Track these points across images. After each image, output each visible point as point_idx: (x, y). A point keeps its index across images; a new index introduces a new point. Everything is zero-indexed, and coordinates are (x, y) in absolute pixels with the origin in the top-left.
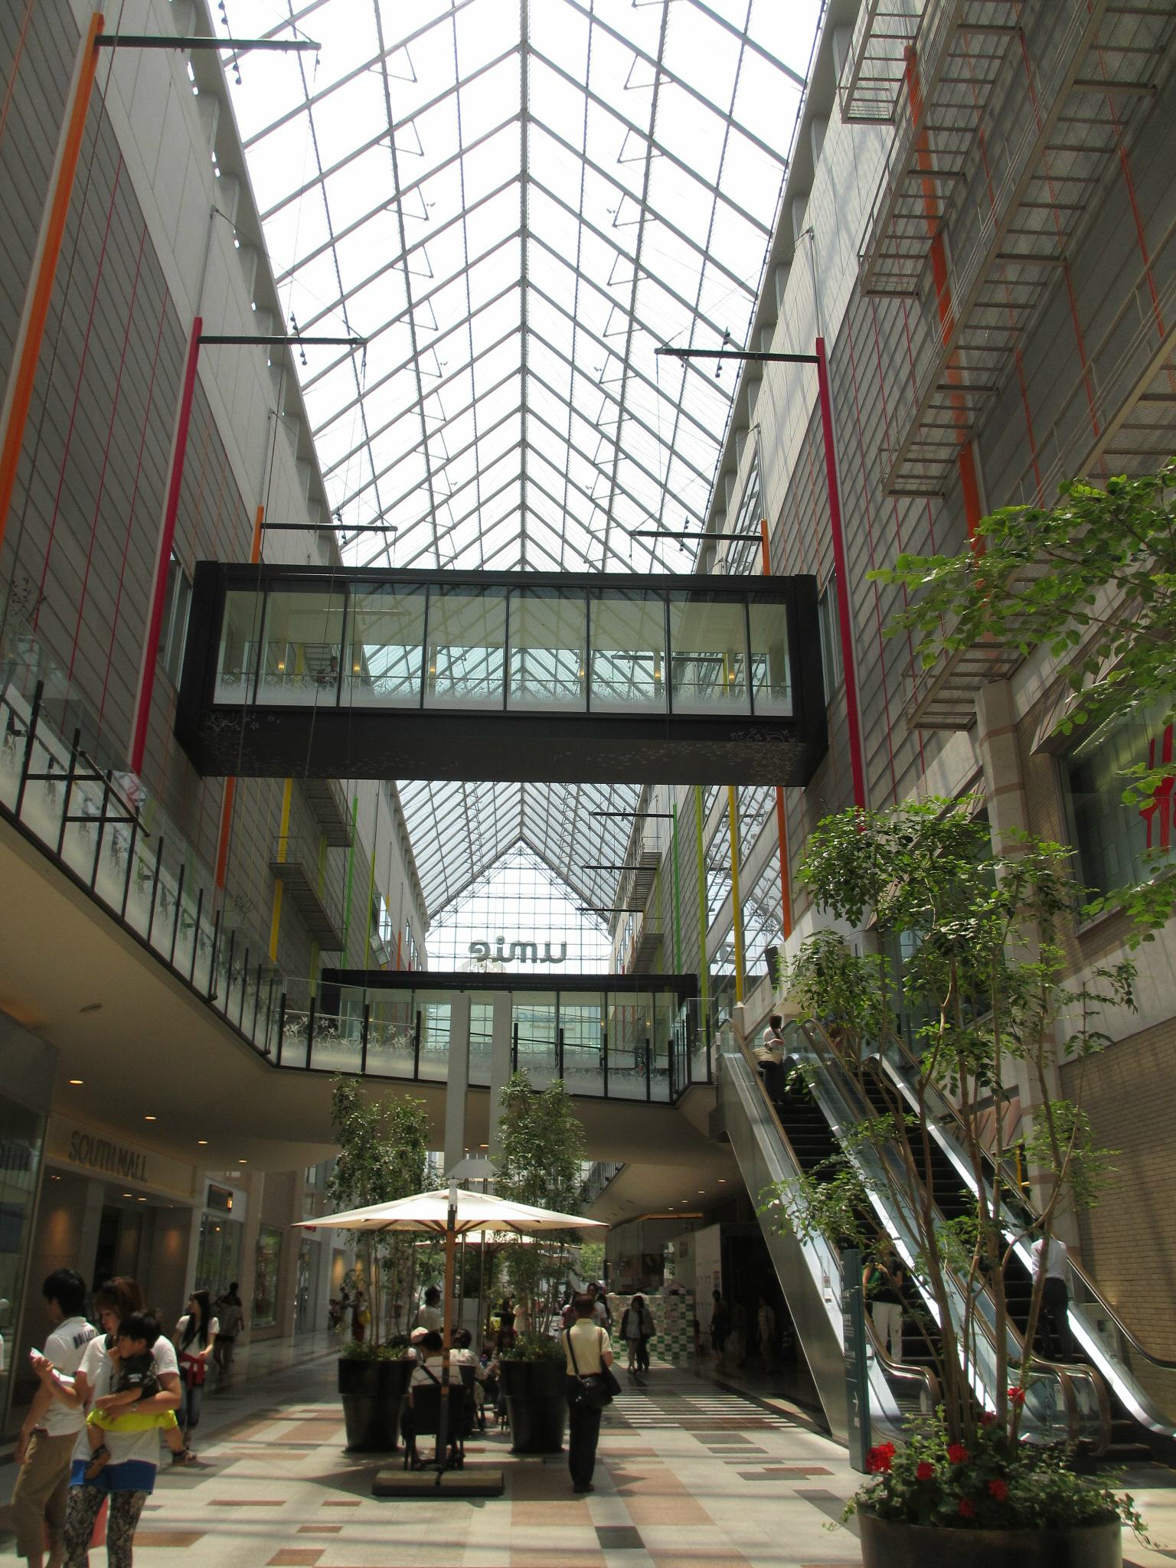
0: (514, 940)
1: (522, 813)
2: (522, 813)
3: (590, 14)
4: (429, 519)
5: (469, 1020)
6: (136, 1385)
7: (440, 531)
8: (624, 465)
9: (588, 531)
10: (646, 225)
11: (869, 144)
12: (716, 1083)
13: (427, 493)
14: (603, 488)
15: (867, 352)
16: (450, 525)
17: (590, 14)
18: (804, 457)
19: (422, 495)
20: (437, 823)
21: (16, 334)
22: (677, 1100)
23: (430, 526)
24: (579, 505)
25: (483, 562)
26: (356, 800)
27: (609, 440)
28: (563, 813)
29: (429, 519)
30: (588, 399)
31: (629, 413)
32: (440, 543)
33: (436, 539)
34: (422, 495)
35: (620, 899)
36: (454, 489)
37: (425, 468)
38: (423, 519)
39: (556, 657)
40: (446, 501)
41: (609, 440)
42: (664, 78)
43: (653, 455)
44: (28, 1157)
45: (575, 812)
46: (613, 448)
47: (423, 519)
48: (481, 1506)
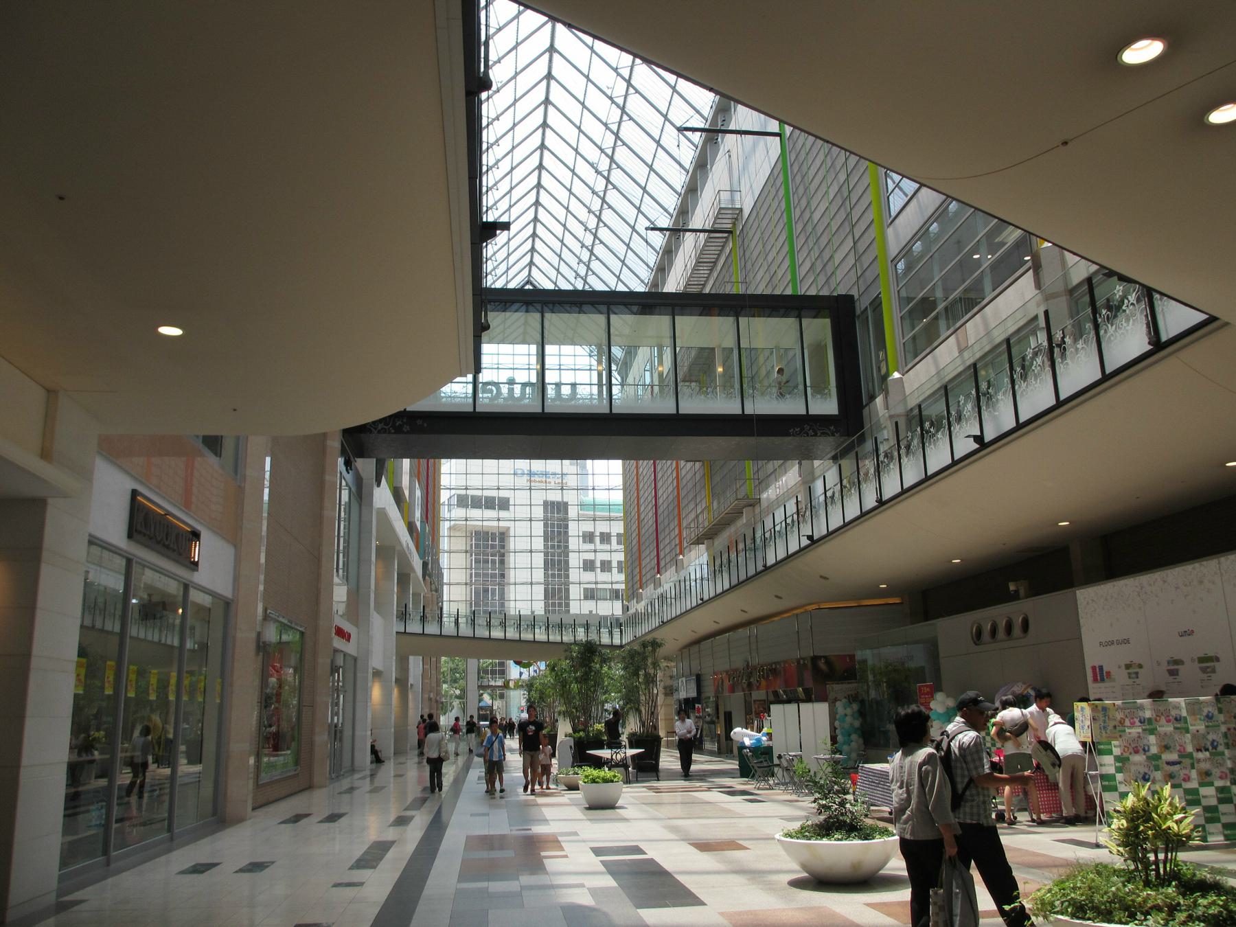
0: (525, 380)
10: (636, 68)
25: (517, 17)
30: (598, 102)
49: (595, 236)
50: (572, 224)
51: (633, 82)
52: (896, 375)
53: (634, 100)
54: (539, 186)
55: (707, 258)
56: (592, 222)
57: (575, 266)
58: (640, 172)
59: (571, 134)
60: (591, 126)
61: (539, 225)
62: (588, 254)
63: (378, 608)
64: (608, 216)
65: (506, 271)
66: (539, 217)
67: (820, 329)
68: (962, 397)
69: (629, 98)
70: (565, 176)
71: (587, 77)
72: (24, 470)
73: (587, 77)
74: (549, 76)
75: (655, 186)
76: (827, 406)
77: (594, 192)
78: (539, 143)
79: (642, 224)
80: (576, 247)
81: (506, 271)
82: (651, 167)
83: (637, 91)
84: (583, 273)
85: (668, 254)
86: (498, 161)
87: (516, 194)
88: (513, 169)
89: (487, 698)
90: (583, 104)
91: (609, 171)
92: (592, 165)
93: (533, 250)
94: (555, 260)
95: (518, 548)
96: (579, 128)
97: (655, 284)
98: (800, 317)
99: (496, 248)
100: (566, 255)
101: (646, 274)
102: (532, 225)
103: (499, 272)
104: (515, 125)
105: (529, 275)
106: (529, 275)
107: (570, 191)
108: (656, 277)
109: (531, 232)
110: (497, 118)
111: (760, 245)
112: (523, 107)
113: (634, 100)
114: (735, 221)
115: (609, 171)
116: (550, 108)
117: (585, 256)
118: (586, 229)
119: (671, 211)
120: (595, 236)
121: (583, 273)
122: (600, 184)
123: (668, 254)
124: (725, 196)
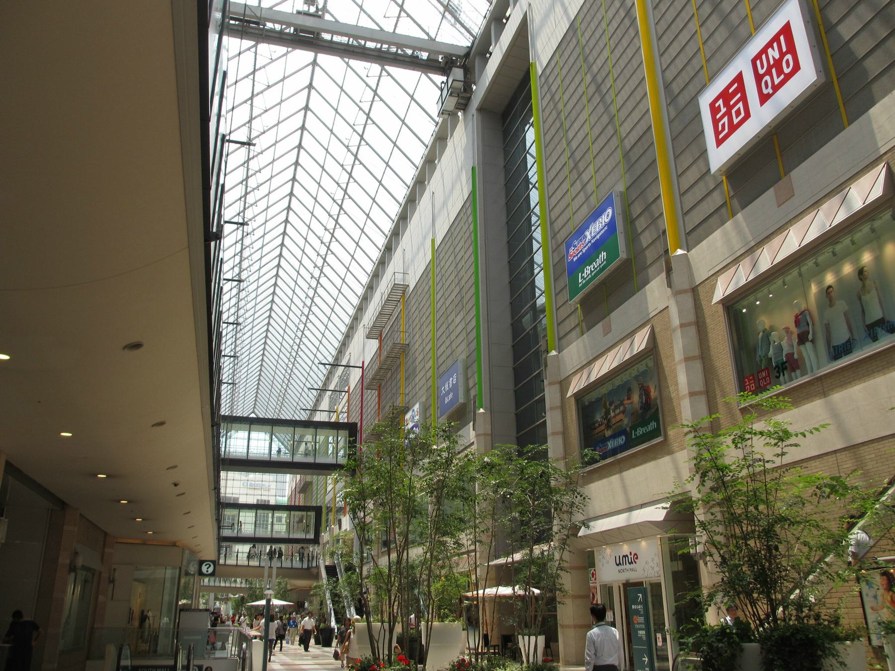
3: (361, 7)
4: (249, 102)
7: (250, 173)
10: (382, 78)
11: (556, 9)
12: (318, 567)
15: (449, 253)
16: (257, 169)
17: (361, 7)
18: (456, 223)
22: (308, 568)
23: (244, 187)
25: (285, 55)
27: (364, 112)
30: (348, 110)
32: (253, 122)
36: (266, 129)
38: (244, 125)
39: (347, 63)
41: (364, 112)
42: (403, 14)
43: (392, 125)
47: (244, 125)
49: (325, 260)
50: (312, 238)
51: (378, 92)
52: (680, 252)
54: (287, 221)
55: (387, 312)
56: (323, 250)
57: (309, 280)
58: (366, 203)
59: (313, 187)
60: (331, 166)
65: (257, 289)
66: (287, 231)
67: (312, 514)
70: (310, 202)
71: (323, 167)
73: (327, 150)
74: (303, 128)
75: (376, 214)
76: (311, 536)
77: (330, 216)
78: (286, 205)
79: (316, 362)
80: (320, 231)
81: (257, 289)
82: (380, 182)
83: (345, 213)
84: (314, 285)
85: (330, 374)
86: (254, 230)
87: (269, 226)
88: (268, 207)
89: (218, 603)
90: (341, 88)
92: (319, 238)
94: (292, 284)
96: (319, 184)
99: (252, 251)
100: (303, 271)
102: (279, 248)
103: (252, 279)
104: (266, 221)
105: (287, 217)
106: (287, 217)
107: (312, 213)
108: (361, 303)
109: (278, 253)
110: (260, 171)
111: (453, 256)
112: (281, 148)
113: (358, 168)
114: (404, 292)
116: (313, 91)
117: (320, 262)
118: (318, 255)
119: (380, 247)
120: (325, 260)
121: (314, 285)
122: (335, 210)
123: (330, 374)
124: (399, 277)
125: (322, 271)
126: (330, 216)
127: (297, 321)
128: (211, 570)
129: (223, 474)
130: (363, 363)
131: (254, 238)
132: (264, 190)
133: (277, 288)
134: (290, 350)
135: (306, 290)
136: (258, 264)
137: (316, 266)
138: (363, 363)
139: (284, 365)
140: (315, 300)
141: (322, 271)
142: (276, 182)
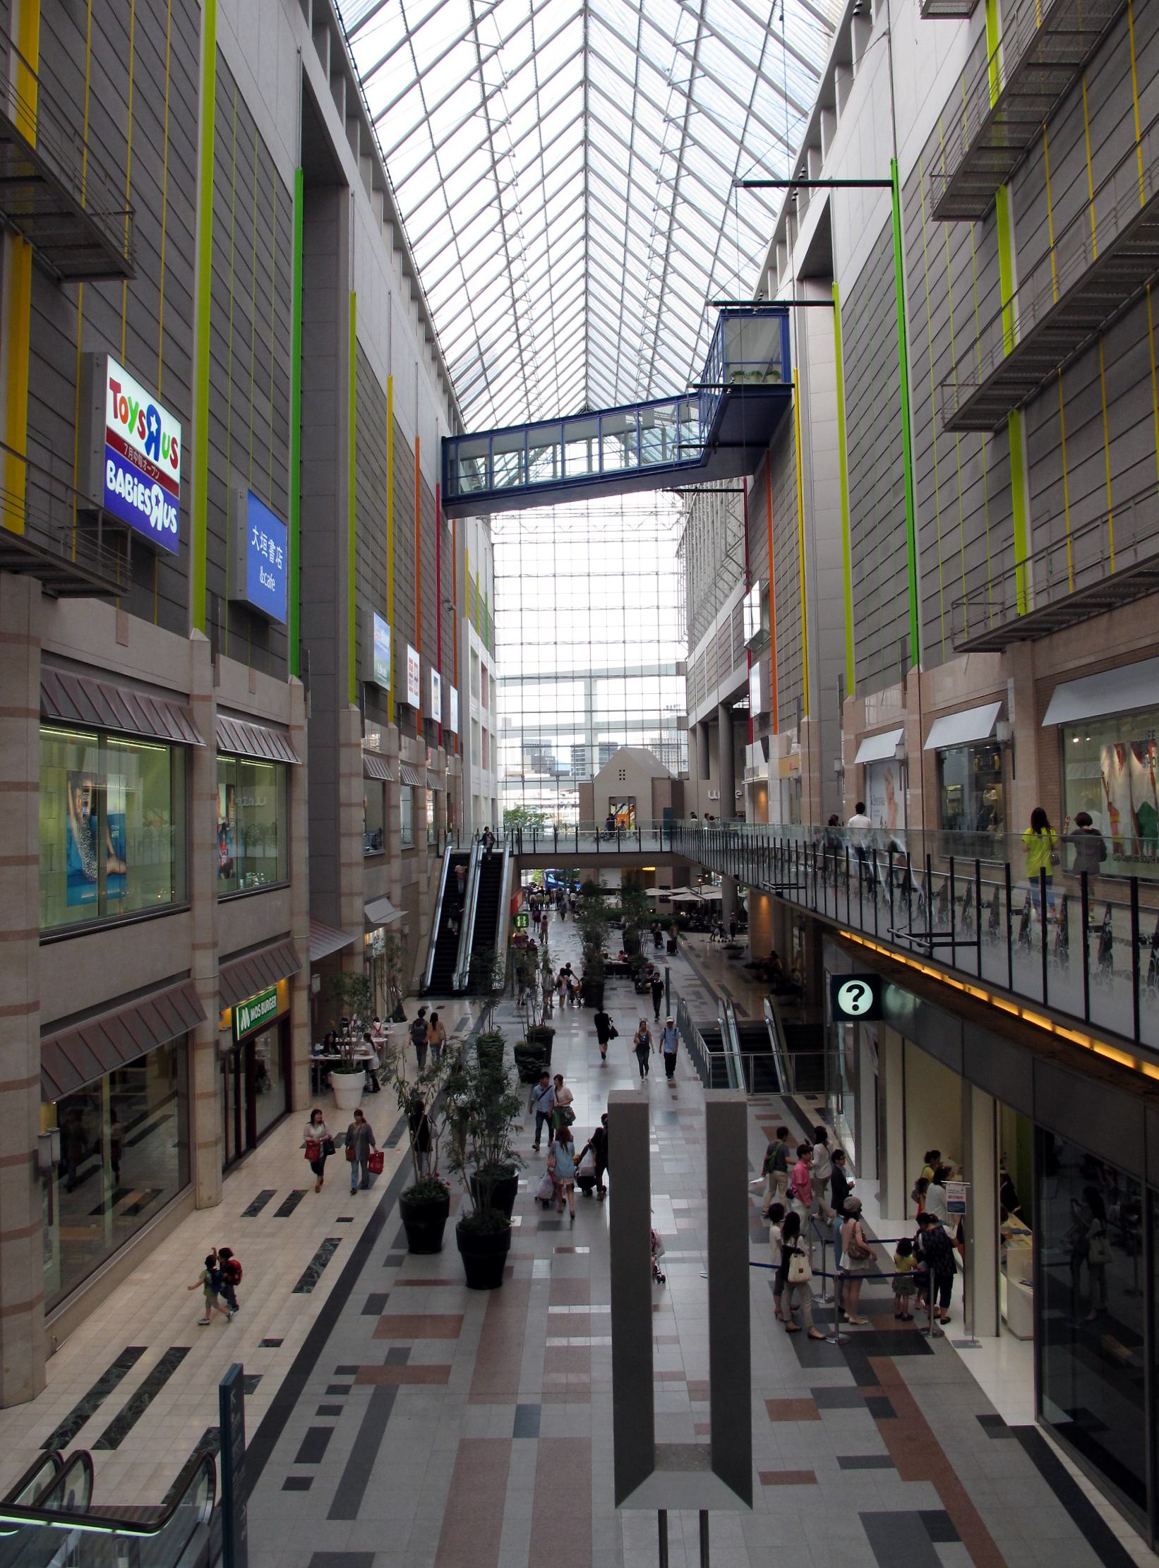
1: (586, 376)
2: (586, 308)
4: (471, 36)
5: (535, 854)
6: (631, 946)
8: (709, 44)
9: (675, 45)
10: (696, 82)
13: (473, 46)
14: (682, 69)
19: (467, 49)
20: (485, 370)
21: (288, 414)
24: (652, 84)
26: (417, 440)
28: (641, 336)
29: (476, 77)
31: (703, 69)
33: (485, 99)
34: (467, 49)
35: (771, 266)
37: (468, 12)
40: (499, 89)
44: (743, 1047)
45: (656, 334)
46: (684, 100)
48: (511, 1268)
50: (643, 145)
53: (710, 47)
56: (670, 169)
58: (742, 79)
61: (591, 151)
62: (688, 64)
63: (475, 764)
64: (698, 125)
68: (651, 892)
69: (692, 119)
72: (980, 1389)
78: (580, 108)
80: (645, 205)
91: (686, 117)
93: (586, 257)
95: (581, 704)
97: (762, 289)
98: (89, 1508)
101: (753, 277)
104: (536, 52)
105: (586, 270)
115: (686, 117)
122: (678, 106)
125: (676, 193)
126: (671, 84)
127: (637, 342)
128: (866, 1003)
129: (619, 870)
130: (894, 163)
131: (519, 164)
132: (522, 85)
133: (591, 282)
134: (636, 359)
135: (651, 215)
136: (547, 298)
137: (665, 151)
138: (894, 163)
139: (632, 353)
140: (661, 333)
141: (676, 193)
142: (547, 62)
